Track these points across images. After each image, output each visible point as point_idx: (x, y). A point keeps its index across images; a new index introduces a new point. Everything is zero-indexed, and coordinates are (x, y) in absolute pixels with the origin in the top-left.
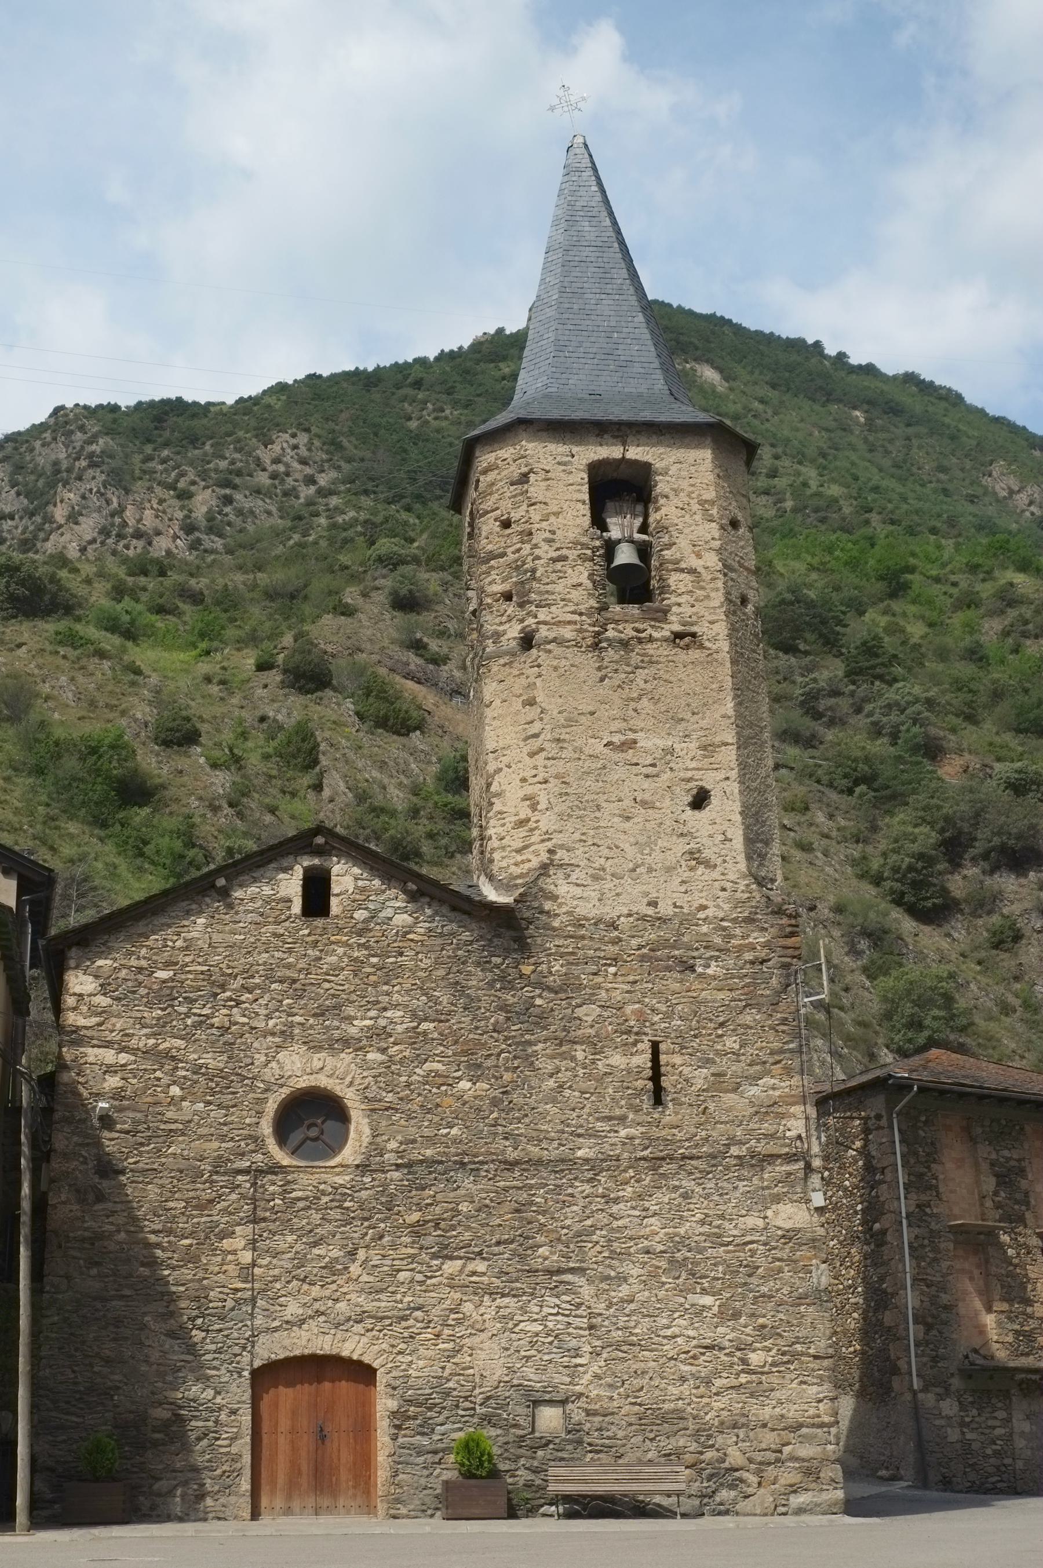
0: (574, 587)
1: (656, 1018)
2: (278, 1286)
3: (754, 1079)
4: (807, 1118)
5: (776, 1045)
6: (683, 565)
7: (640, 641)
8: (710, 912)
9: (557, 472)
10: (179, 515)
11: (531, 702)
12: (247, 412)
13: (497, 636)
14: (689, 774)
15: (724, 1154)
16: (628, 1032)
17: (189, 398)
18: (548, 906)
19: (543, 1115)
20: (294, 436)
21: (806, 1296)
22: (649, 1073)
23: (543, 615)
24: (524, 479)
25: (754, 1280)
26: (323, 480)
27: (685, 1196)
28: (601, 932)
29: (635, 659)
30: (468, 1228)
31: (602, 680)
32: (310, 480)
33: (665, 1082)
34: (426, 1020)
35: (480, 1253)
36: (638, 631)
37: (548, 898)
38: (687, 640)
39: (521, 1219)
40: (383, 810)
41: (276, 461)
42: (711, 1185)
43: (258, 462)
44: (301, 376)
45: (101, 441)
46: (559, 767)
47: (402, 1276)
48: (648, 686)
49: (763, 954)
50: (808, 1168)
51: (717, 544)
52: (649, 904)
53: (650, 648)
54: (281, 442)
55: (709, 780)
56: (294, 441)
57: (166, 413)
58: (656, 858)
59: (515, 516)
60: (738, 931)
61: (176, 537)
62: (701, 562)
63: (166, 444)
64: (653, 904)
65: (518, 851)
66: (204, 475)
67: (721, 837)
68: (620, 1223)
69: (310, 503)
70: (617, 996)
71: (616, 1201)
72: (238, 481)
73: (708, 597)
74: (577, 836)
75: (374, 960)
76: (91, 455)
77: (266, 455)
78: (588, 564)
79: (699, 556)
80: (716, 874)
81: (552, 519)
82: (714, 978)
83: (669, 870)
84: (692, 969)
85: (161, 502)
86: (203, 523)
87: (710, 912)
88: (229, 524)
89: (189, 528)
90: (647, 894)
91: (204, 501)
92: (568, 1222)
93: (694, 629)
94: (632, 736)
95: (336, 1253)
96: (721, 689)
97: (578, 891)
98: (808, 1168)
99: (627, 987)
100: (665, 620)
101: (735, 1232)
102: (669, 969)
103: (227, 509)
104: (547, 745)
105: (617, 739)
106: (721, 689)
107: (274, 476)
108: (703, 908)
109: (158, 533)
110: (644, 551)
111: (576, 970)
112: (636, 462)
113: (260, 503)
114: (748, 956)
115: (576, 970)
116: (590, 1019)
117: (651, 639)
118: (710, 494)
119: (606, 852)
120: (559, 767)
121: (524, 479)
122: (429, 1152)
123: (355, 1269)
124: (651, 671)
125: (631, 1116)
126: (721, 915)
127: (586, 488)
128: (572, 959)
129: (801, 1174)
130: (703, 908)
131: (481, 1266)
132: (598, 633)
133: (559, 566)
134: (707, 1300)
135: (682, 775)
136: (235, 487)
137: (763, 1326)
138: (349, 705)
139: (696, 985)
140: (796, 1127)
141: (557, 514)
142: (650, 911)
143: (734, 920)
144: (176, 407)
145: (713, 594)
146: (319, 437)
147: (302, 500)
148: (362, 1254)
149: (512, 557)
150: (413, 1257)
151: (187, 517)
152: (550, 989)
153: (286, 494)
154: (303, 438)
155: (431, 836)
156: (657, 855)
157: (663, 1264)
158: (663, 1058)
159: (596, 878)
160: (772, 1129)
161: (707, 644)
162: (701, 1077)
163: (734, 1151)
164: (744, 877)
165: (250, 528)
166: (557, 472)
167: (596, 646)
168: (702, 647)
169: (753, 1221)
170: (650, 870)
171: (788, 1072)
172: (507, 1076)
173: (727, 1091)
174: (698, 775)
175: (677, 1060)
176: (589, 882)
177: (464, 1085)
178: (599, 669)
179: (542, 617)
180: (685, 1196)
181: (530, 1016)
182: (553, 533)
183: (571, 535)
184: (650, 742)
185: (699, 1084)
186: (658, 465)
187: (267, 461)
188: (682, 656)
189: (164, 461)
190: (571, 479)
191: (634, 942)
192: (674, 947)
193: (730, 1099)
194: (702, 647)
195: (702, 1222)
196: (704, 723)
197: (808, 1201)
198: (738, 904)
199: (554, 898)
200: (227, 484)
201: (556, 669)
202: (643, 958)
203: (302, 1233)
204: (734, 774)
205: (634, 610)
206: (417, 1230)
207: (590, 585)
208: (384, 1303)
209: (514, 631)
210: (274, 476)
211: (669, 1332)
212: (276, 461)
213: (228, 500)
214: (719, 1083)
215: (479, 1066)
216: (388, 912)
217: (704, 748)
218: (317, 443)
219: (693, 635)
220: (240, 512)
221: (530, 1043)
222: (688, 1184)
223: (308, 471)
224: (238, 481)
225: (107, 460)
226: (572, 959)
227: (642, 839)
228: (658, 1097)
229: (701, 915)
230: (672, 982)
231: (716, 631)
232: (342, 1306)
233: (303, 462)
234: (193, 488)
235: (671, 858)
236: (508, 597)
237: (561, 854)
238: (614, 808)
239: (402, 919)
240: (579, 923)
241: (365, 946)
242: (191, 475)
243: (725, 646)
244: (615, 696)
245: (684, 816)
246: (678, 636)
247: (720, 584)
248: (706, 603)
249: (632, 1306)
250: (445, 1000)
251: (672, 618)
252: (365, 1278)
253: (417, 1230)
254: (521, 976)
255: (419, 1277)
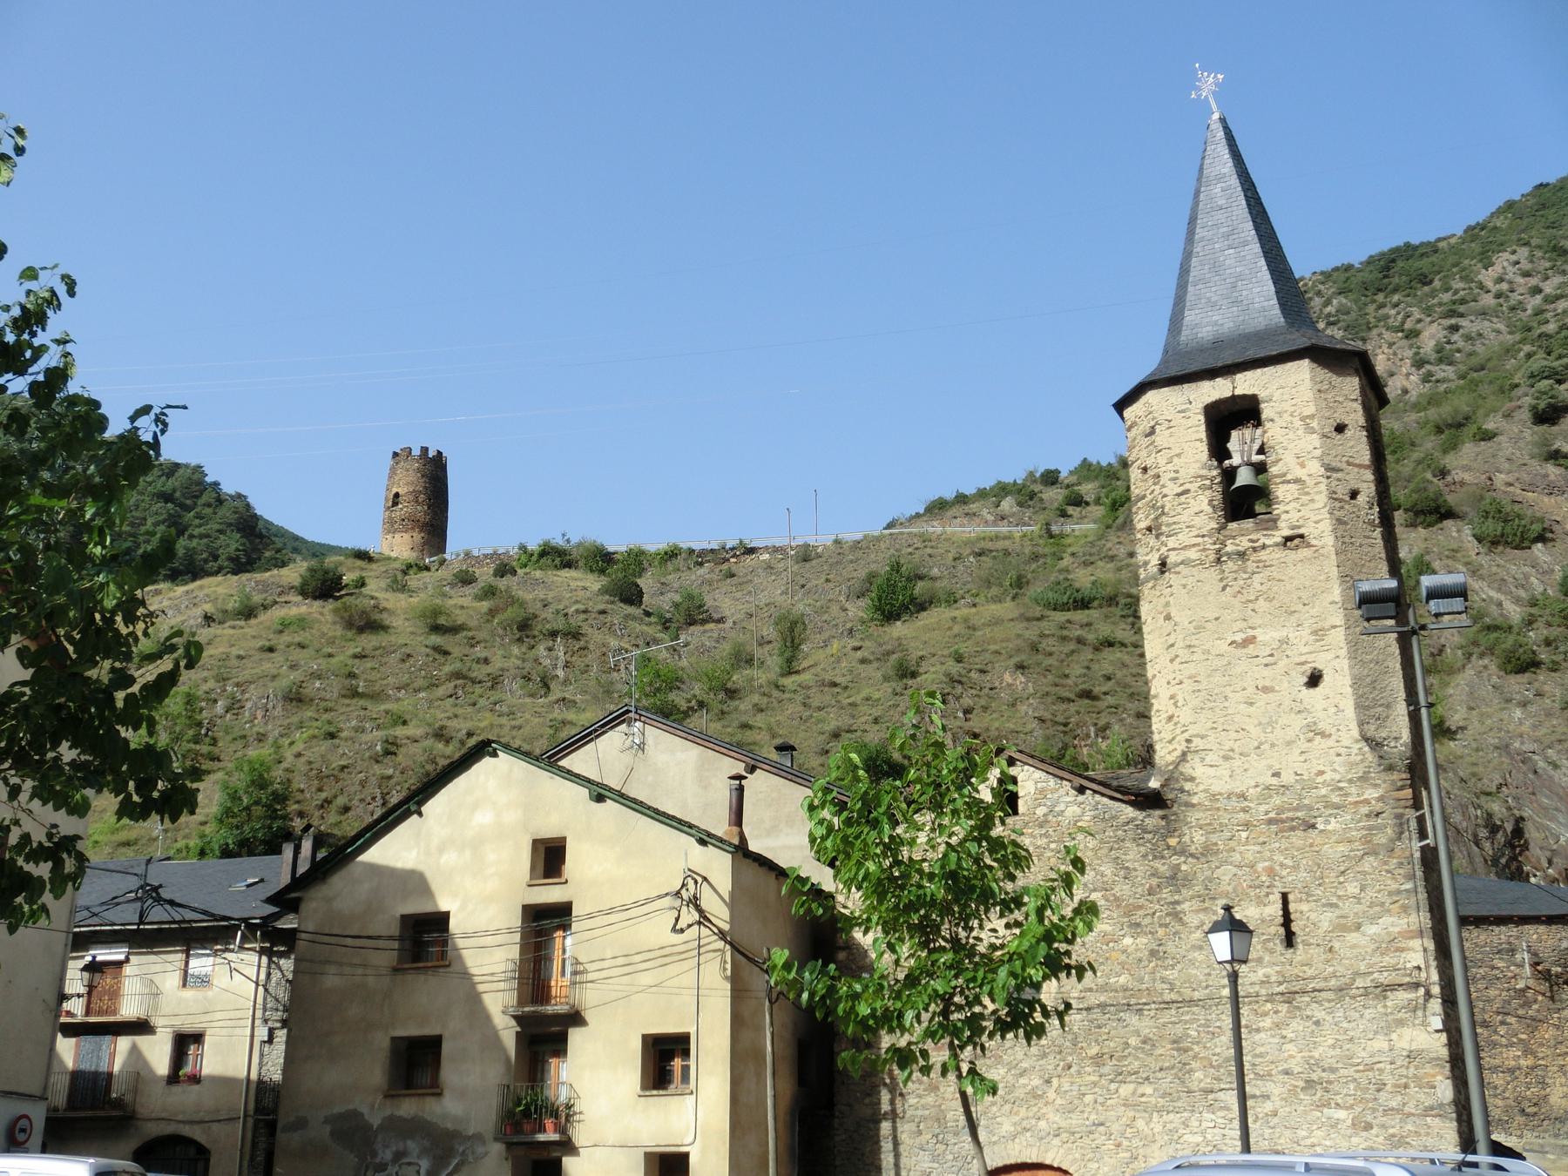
0: (1198, 510)
1: (1284, 873)
2: (994, 1109)
3: (1373, 919)
4: (1425, 950)
5: (1395, 886)
6: (1289, 477)
7: (1255, 549)
8: (1327, 777)
9: (1178, 419)
10: (1409, 353)
11: (1168, 618)
12: (1474, 238)
13: (1146, 563)
14: (1303, 659)
15: (1348, 987)
16: (1259, 887)
17: (1415, 241)
18: (1187, 786)
19: (1192, 962)
20: (1514, 252)
21: (1432, 1108)
22: (1281, 920)
23: (1172, 542)
24: (1152, 432)
25: (1383, 1096)
26: (1549, 288)
27: (1317, 1023)
28: (1234, 803)
29: (1251, 566)
30: (1137, 1058)
31: (1224, 589)
32: (1537, 290)
33: (1294, 927)
34: (1095, 890)
35: (1147, 1079)
36: (1252, 541)
37: (1186, 780)
38: (1296, 541)
39: (1178, 1050)
40: (1496, 628)
41: (1500, 280)
42: (1340, 1014)
43: (1481, 286)
44: (1527, 189)
45: (1335, 302)
46: (1190, 669)
47: (1088, 1099)
48: (1264, 588)
49: (1379, 806)
50: (1428, 995)
51: (1318, 453)
52: (1274, 775)
53: (1263, 555)
54: (1502, 261)
55: (1321, 662)
56: (1514, 258)
57: (1393, 261)
58: (1278, 735)
59: (1149, 463)
60: (1353, 790)
61: (1408, 374)
62: (1305, 471)
63: (1395, 290)
64: (1276, 774)
65: (1170, 742)
66: (1428, 311)
67: (1334, 710)
68: (1262, 1049)
69: (1539, 312)
70: (1250, 856)
71: (1258, 1030)
72: (1462, 309)
73: (1312, 501)
74: (1209, 725)
75: (1053, 846)
76: (1329, 315)
77: (1487, 277)
78: (1208, 493)
79: (1303, 465)
80: (1331, 742)
81: (1176, 460)
82: (1334, 832)
83: (1289, 743)
84: (1313, 826)
85: (1391, 345)
86: (1433, 356)
87: (1327, 777)
88: (1459, 351)
89: (1419, 363)
90: (1270, 767)
91: (1431, 335)
92: (1218, 1050)
93: (1301, 531)
94: (1251, 633)
95: (1036, 1082)
96: (1327, 579)
97: (1211, 771)
98: (1428, 995)
99: (1257, 848)
100: (1276, 528)
101: (1363, 1054)
102: (1293, 829)
103: (1455, 337)
104: (1180, 652)
105: (1239, 637)
106: (1327, 579)
107: (1498, 296)
108: (1321, 773)
109: (1392, 375)
110: (1260, 468)
111: (1214, 838)
112: (1244, 396)
113: (1487, 323)
114: (1365, 810)
115: (1214, 838)
116: (1227, 878)
117: (1264, 547)
118: (1311, 410)
119: (1233, 735)
120: (1190, 669)
121: (1152, 432)
122: (1102, 999)
123: (1051, 1095)
124: (1267, 572)
125: (1267, 958)
126: (1338, 777)
127: (1203, 428)
128: (1209, 828)
129: (1421, 1001)
130: (1321, 773)
131: (1148, 1090)
132: (1219, 551)
133: (1183, 498)
134: (1342, 1114)
135: (1298, 660)
136: (1462, 315)
137: (1393, 1136)
138: (1467, 531)
139: (1319, 840)
140: (1416, 958)
141: (1179, 455)
142: (1274, 781)
143: (1350, 781)
144: (1407, 251)
145: (1317, 497)
146: (1540, 247)
147: (1529, 312)
148: (1055, 1081)
149: (1150, 497)
150: (1095, 1084)
151: (1417, 354)
152: (1192, 855)
153: (1513, 309)
154: (1523, 252)
155: (1548, 643)
156: (1278, 731)
157: (1301, 1084)
158: (1292, 907)
159: (1226, 758)
160: (1393, 961)
161: (1313, 542)
162: (1326, 919)
163: (1360, 983)
164: (1357, 741)
165: (1479, 348)
166: (1178, 419)
167: (1218, 561)
168: (1309, 545)
169: (1380, 1043)
170: (1273, 745)
171: (1405, 909)
172: (1161, 932)
173: (1350, 931)
174: (1310, 658)
175: (1304, 907)
176: (1221, 761)
177: (1128, 941)
178: (1221, 580)
179: (1171, 545)
180: (1317, 1023)
181: (1175, 879)
182: (1177, 472)
183: (1192, 472)
184: (1267, 636)
185: (1325, 925)
186: (1262, 395)
187: (1489, 284)
188: (1291, 556)
189: (1396, 305)
190: (1190, 423)
191: (1263, 808)
192: (1296, 809)
193: (1353, 937)
194: (1309, 545)
195: (1333, 1047)
196: (1314, 612)
197: (1429, 1025)
198: (1352, 765)
199: (1192, 779)
200: (1452, 313)
201: (1184, 586)
202: (1270, 822)
203: (1011, 1067)
204: (1343, 652)
205: (1248, 524)
206: (1098, 1060)
207: (1210, 510)
208: (1075, 1121)
209: (1154, 560)
210: (1498, 296)
211: (1308, 1142)
212: (1500, 280)
213: (1455, 329)
214: (1342, 928)
215: (1138, 925)
216: (1061, 807)
217: (1315, 633)
218: (1539, 254)
219: (1302, 536)
220: (1468, 338)
221: (1177, 903)
222: (1319, 1014)
223: (1533, 281)
224: (1462, 309)
225: (1342, 317)
226: (1209, 828)
227: (1264, 721)
228: (1289, 940)
229: (1320, 779)
230: (1297, 838)
231: (1321, 530)
232: (1042, 1124)
233: (1526, 274)
234: (1419, 326)
235: (1290, 734)
236: (1149, 529)
237: (1197, 742)
238: (1239, 696)
239: (1073, 811)
240: (1214, 797)
241: (1046, 835)
242: (1417, 314)
243: (1329, 540)
244: (1236, 602)
245: (1300, 696)
246: (1288, 539)
247: (1323, 487)
248: (1312, 506)
249: (1276, 1120)
250: (1108, 872)
251: (1281, 524)
252: (1059, 1101)
253: (1098, 1060)
254: (1169, 847)
255: (1100, 1099)
